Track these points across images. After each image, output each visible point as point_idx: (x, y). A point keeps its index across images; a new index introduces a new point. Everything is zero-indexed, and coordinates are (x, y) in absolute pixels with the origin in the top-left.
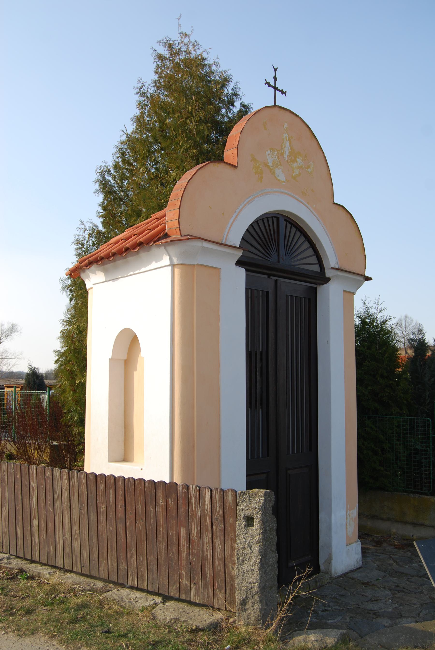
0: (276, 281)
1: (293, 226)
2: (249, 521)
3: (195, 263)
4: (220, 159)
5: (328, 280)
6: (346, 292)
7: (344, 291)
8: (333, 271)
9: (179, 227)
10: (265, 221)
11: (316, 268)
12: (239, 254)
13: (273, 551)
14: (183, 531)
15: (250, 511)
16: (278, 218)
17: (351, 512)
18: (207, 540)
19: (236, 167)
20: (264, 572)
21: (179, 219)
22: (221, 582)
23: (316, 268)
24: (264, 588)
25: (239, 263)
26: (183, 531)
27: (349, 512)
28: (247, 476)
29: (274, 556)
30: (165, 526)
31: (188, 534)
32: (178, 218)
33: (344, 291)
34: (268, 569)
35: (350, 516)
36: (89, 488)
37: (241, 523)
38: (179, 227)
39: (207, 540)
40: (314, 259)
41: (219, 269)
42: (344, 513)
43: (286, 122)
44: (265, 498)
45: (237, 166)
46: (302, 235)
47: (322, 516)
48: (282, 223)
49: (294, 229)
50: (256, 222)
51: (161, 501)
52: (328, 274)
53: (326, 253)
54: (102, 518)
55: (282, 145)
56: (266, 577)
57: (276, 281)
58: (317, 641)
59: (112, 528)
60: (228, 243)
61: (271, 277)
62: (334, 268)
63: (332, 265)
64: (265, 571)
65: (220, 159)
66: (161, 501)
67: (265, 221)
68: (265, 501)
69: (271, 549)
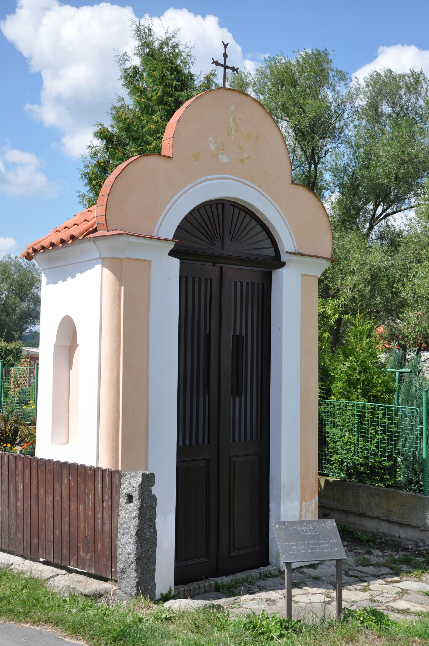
0: (221, 268)
1: (241, 211)
2: (130, 498)
3: (124, 257)
4: (157, 151)
5: (283, 264)
6: (306, 275)
7: (302, 275)
8: (288, 255)
9: (106, 223)
10: (208, 208)
11: (271, 252)
12: (171, 246)
13: (152, 526)
14: (81, 507)
15: (130, 490)
16: (223, 204)
17: (308, 503)
18: (99, 516)
19: (171, 158)
20: (139, 544)
21: (105, 215)
22: (107, 553)
23: (271, 252)
24: (140, 559)
25: (172, 253)
26: (81, 507)
27: (304, 503)
28: (178, 462)
29: (152, 531)
30: (68, 502)
31: (85, 509)
32: (104, 214)
33: (302, 275)
34: (144, 542)
35: (305, 507)
36: (10, 467)
37: (123, 500)
38: (106, 223)
39: (99, 516)
40: (268, 243)
41: (150, 261)
42: (297, 504)
43: (233, 104)
44: (142, 478)
45: (172, 157)
46: (253, 219)
47: (272, 506)
48: (229, 210)
49: (243, 214)
50: (197, 209)
51: (66, 481)
52: (284, 258)
53: (280, 237)
54: (20, 496)
55: (228, 129)
56: (142, 549)
57: (221, 268)
58: (226, 621)
59: (27, 505)
60: (161, 236)
61: (216, 264)
62: (287, 252)
63: (287, 250)
64: (141, 543)
65: (157, 151)
66: (66, 481)
67: (208, 208)
68: (143, 481)
69: (148, 525)
